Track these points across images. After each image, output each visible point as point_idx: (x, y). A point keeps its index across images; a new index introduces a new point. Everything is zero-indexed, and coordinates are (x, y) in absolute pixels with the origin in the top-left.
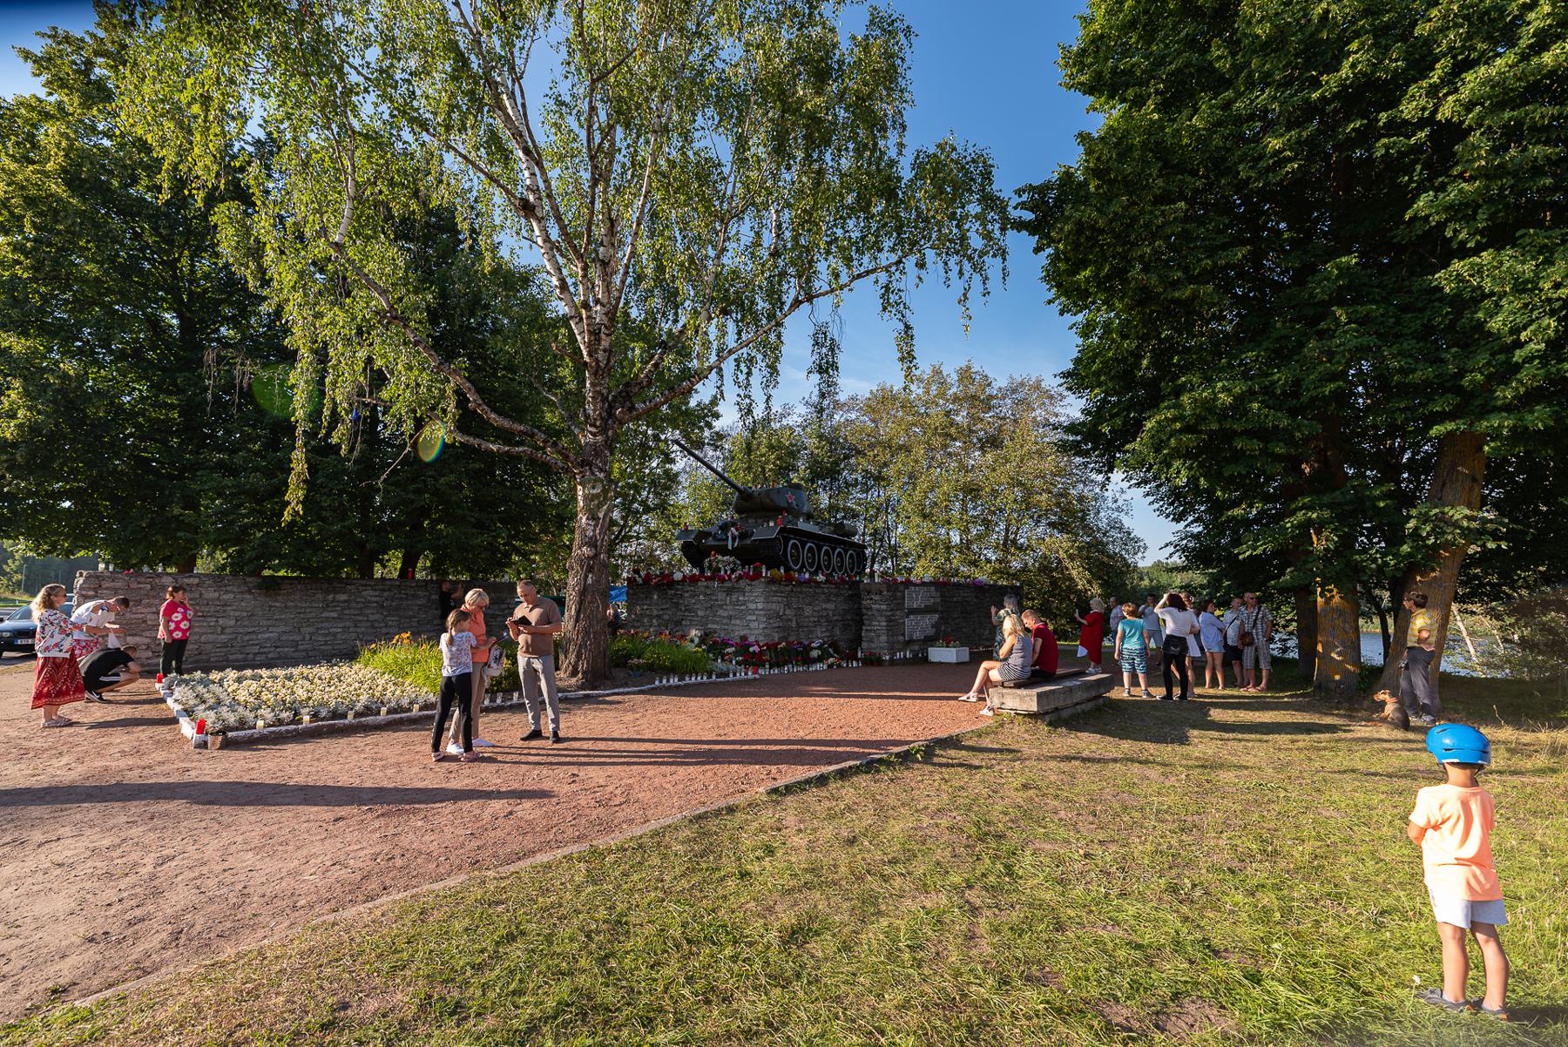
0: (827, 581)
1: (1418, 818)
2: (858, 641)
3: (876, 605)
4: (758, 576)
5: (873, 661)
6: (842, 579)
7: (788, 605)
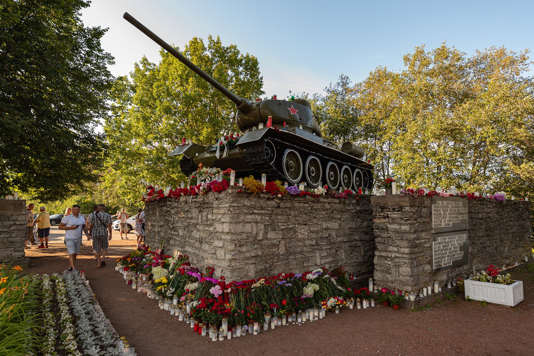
0: (328, 194)
2: (368, 268)
3: (394, 226)
4: (225, 184)
5: (390, 301)
6: (348, 193)
7: (271, 226)
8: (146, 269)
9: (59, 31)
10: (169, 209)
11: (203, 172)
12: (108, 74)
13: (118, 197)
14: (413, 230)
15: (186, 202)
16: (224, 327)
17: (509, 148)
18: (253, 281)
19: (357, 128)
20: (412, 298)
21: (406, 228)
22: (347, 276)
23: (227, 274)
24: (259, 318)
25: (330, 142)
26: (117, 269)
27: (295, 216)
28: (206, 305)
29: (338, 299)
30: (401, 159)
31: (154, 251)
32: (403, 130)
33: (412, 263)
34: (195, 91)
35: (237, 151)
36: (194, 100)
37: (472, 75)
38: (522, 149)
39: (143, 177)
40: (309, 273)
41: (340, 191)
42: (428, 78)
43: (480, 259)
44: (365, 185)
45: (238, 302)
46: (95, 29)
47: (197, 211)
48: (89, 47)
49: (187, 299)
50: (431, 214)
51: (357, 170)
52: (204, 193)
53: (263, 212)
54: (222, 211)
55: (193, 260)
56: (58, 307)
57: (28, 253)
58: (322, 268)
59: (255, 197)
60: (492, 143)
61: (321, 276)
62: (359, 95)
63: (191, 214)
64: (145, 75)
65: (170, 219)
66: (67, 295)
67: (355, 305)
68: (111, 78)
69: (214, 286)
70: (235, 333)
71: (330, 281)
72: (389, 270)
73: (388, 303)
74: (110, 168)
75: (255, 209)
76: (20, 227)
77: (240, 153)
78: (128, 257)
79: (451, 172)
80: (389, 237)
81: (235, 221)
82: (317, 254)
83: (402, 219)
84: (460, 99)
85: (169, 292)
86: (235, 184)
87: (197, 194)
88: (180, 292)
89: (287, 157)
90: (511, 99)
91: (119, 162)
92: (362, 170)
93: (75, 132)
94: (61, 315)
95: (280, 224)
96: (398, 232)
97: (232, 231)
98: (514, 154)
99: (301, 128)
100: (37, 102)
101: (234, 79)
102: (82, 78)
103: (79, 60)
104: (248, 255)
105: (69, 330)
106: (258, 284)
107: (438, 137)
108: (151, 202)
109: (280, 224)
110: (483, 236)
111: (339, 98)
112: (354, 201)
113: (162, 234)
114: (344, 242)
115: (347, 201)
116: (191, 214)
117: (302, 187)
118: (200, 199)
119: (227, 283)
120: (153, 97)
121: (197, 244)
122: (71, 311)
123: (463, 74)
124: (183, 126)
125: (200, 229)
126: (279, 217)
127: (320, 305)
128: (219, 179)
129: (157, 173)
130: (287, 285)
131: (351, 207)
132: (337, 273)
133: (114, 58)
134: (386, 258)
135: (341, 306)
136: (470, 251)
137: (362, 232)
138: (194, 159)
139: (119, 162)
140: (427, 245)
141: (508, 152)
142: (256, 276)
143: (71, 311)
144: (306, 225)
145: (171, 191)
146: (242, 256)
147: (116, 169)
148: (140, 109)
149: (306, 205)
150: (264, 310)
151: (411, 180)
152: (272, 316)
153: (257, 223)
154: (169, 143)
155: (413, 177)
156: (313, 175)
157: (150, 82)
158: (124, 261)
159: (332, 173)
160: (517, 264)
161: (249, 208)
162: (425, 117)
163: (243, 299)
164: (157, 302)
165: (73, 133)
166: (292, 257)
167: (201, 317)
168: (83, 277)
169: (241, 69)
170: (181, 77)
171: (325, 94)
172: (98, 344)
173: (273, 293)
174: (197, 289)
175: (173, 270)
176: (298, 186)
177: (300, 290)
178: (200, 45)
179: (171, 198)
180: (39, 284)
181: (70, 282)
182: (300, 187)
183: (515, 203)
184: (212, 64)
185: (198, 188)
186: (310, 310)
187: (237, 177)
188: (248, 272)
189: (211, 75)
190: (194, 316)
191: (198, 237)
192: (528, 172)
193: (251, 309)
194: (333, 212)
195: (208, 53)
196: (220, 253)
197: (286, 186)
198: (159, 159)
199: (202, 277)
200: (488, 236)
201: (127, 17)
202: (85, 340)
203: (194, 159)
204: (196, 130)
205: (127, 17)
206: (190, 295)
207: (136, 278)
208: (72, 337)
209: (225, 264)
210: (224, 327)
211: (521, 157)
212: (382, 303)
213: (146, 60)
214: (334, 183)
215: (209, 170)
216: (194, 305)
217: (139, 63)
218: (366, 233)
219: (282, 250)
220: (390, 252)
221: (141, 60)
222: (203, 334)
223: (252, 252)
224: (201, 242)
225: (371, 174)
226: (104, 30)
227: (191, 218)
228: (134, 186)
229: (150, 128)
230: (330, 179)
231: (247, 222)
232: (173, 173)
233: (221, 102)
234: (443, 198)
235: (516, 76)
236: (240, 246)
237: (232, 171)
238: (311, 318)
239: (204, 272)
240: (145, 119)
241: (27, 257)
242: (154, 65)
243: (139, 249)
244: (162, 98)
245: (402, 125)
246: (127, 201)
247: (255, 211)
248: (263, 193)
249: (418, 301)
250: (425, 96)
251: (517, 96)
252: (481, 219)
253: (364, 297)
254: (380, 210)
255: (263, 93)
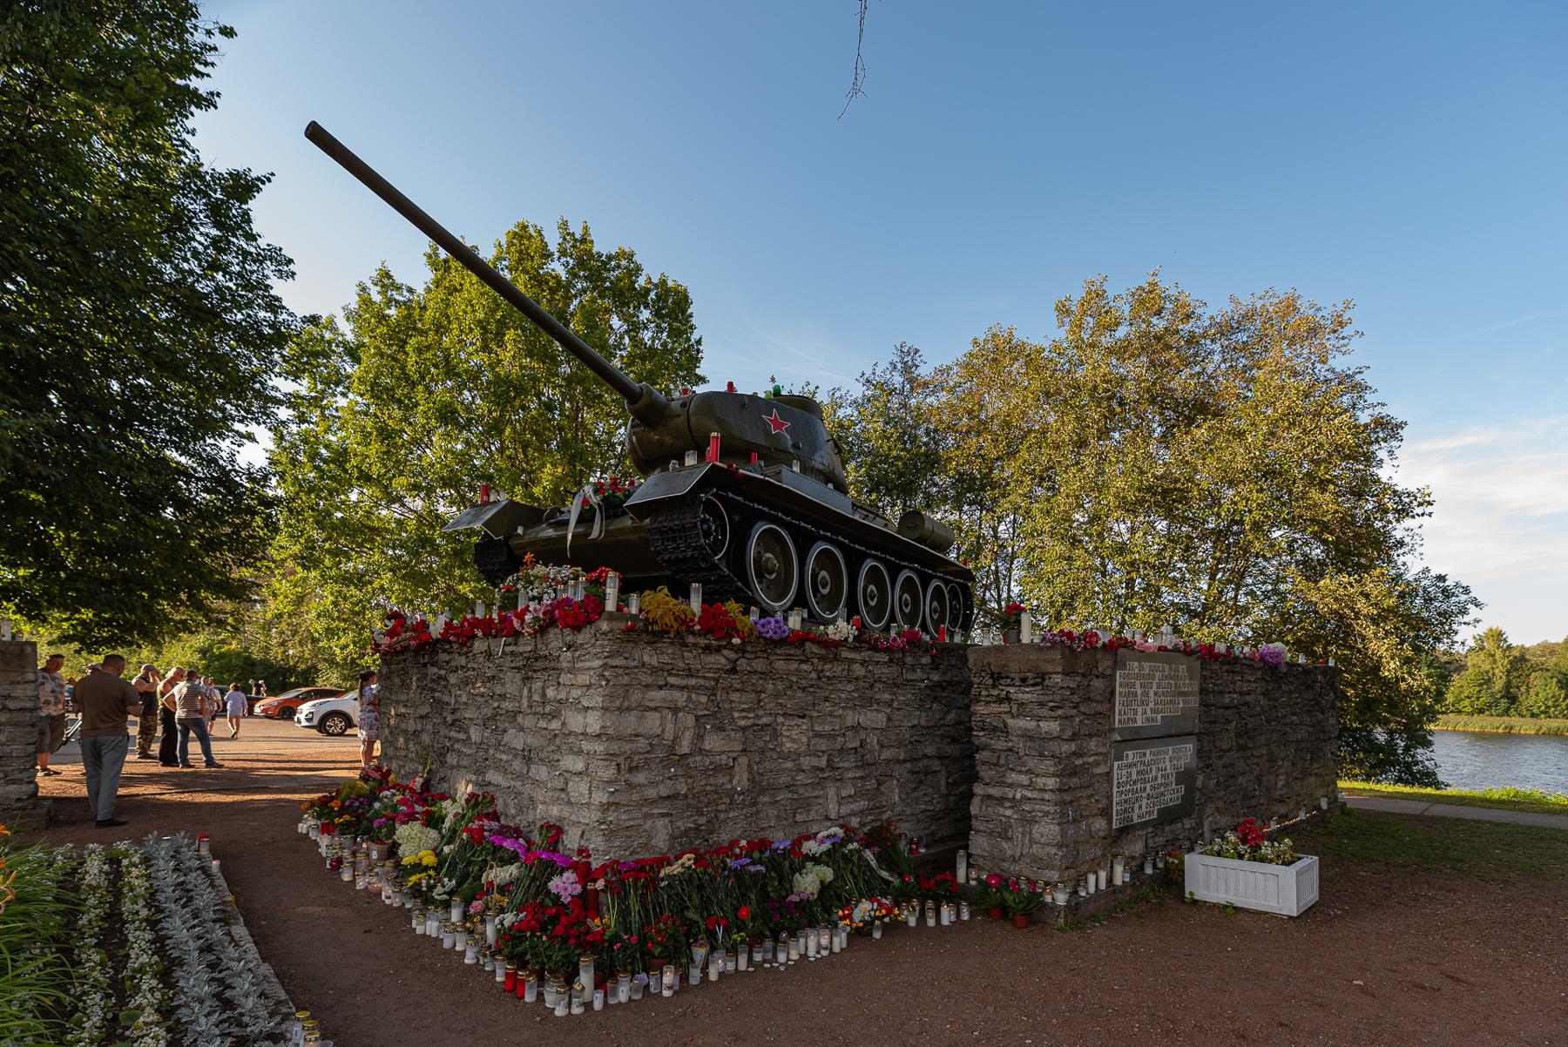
1: (1184, 754)
2: (955, 826)
3: (1023, 720)
4: (592, 608)
5: (1009, 907)
6: (913, 640)
7: (715, 719)
8: (380, 828)
9: (128, 174)
10: (443, 672)
11: (536, 577)
12: (274, 305)
13: (314, 641)
14: (1069, 733)
15: (489, 654)
16: (586, 978)
17: (1295, 540)
18: (663, 861)
19: (937, 479)
20: (1061, 898)
21: (1051, 727)
22: (903, 845)
23: (596, 842)
24: (677, 955)
25: (873, 510)
26: (302, 828)
27: (776, 695)
28: (539, 922)
29: (880, 904)
30: (1041, 560)
31: (405, 782)
32: (1048, 489)
33: (1063, 814)
34: (522, 368)
35: (627, 522)
36: (520, 390)
37: (1217, 358)
38: (1325, 542)
39: (382, 589)
40: (808, 838)
41: (893, 633)
42: (1114, 362)
43: (1220, 804)
44: (954, 622)
45: (624, 913)
46: (236, 176)
47: (518, 677)
48: (217, 225)
49: (488, 908)
50: (1113, 693)
51: (935, 583)
52: (536, 632)
53: (693, 682)
54: (583, 679)
55: (506, 805)
56: (121, 932)
57: (47, 785)
58: (842, 827)
59: (672, 643)
60: (1257, 526)
61: (838, 845)
62: (944, 396)
63: (503, 685)
64: (385, 317)
65: (446, 698)
66: (151, 899)
67: (922, 918)
68: (285, 316)
69: (561, 874)
70: (615, 993)
71: (861, 858)
72: (1006, 831)
73: (1002, 912)
74: (290, 564)
75: (670, 675)
76: (20, 717)
77: (635, 529)
78: (332, 798)
79: (1158, 594)
80: (1010, 750)
81: (617, 705)
82: (831, 792)
83: (1042, 704)
84: (1186, 417)
85: (439, 889)
86: (619, 609)
87: (517, 634)
88: (470, 890)
89: (758, 544)
90: (1307, 422)
91: (313, 548)
92: (947, 582)
93: (183, 460)
94: (128, 956)
95: (736, 715)
96: (1031, 738)
97: (610, 731)
98: (1304, 555)
99: (796, 469)
100: (70, 370)
101: (627, 340)
102: (196, 311)
103: (186, 260)
104: (652, 793)
105: (147, 995)
106: (676, 869)
107: (1130, 508)
108: (397, 653)
109: (736, 715)
110: (1230, 750)
111: (895, 401)
112: (926, 660)
113: (425, 738)
114: (898, 761)
115: (909, 660)
116: (503, 685)
117: (795, 621)
118: (525, 646)
119: (594, 866)
120: (407, 378)
121: (517, 765)
122: (160, 944)
123: (1196, 355)
124: (491, 459)
125: (527, 724)
126: (735, 696)
127: (835, 917)
128: (577, 593)
129: (418, 580)
130: (752, 869)
131: (919, 674)
132: (880, 837)
133: (290, 261)
134: (1001, 800)
135: (887, 920)
136: (1199, 784)
137: (942, 737)
138: (513, 542)
139: (313, 548)
140: (1099, 770)
141: (1291, 551)
142: (672, 847)
143: (160, 944)
144: (803, 717)
145: (448, 625)
146: (635, 797)
147: (304, 567)
148: (372, 409)
149: (804, 667)
150: (690, 934)
151: (1064, 613)
152: (713, 949)
153: (675, 710)
154: (452, 503)
155: (1069, 605)
156: (825, 591)
157: (399, 335)
158: (322, 808)
159: (872, 587)
160: (1302, 816)
161: (654, 670)
162: (1102, 459)
163: (635, 906)
164: (406, 915)
165: (178, 463)
166: (767, 799)
167: (524, 953)
168: (204, 851)
169: (645, 314)
170: (483, 328)
171: (858, 391)
172: (229, 1034)
173: (715, 891)
174: (515, 882)
175: (454, 832)
176: (786, 619)
177: (786, 883)
178: (536, 243)
179: (450, 643)
180: (75, 870)
181: (164, 866)
182: (791, 619)
183: (1306, 671)
184: (568, 299)
185: (521, 617)
186: (808, 931)
187: (625, 590)
188: (650, 837)
189: (567, 325)
190: (506, 951)
191: (519, 746)
192: (1336, 599)
193: (658, 932)
194: (872, 686)
195: (557, 268)
196: (578, 789)
197: (754, 617)
198: (425, 542)
199: (528, 850)
200: (1242, 748)
201: (316, 134)
202: (191, 1022)
203: (513, 542)
204: (524, 471)
205: (316, 134)
206: (496, 896)
207: (354, 854)
208: (155, 1018)
209: (590, 817)
210: (586, 978)
211: (1322, 563)
212: (987, 912)
213: (388, 275)
214: (877, 614)
215: (552, 571)
216: (507, 923)
217: (369, 284)
218: (954, 741)
219: (741, 780)
220: (1010, 785)
221: (375, 274)
222: (529, 997)
223: (661, 787)
224: (528, 760)
225: (968, 595)
226: (258, 179)
227: (503, 697)
228: (357, 614)
229: (397, 461)
230: (866, 604)
231: (651, 709)
232: (462, 579)
233: (593, 400)
234: (1144, 655)
235: (1319, 366)
236: (631, 770)
237: (611, 574)
238: (812, 953)
239: (536, 838)
240: (385, 434)
241: (45, 798)
242: (410, 291)
243: (365, 778)
244: (432, 380)
245: (1045, 477)
246: (338, 651)
247: (671, 680)
248: (693, 633)
249: (1074, 907)
250: (1105, 404)
251: (1319, 415)
252: (1227, 708)
253: (944, 897)
254: (990, 682)
255: (702, 380)
